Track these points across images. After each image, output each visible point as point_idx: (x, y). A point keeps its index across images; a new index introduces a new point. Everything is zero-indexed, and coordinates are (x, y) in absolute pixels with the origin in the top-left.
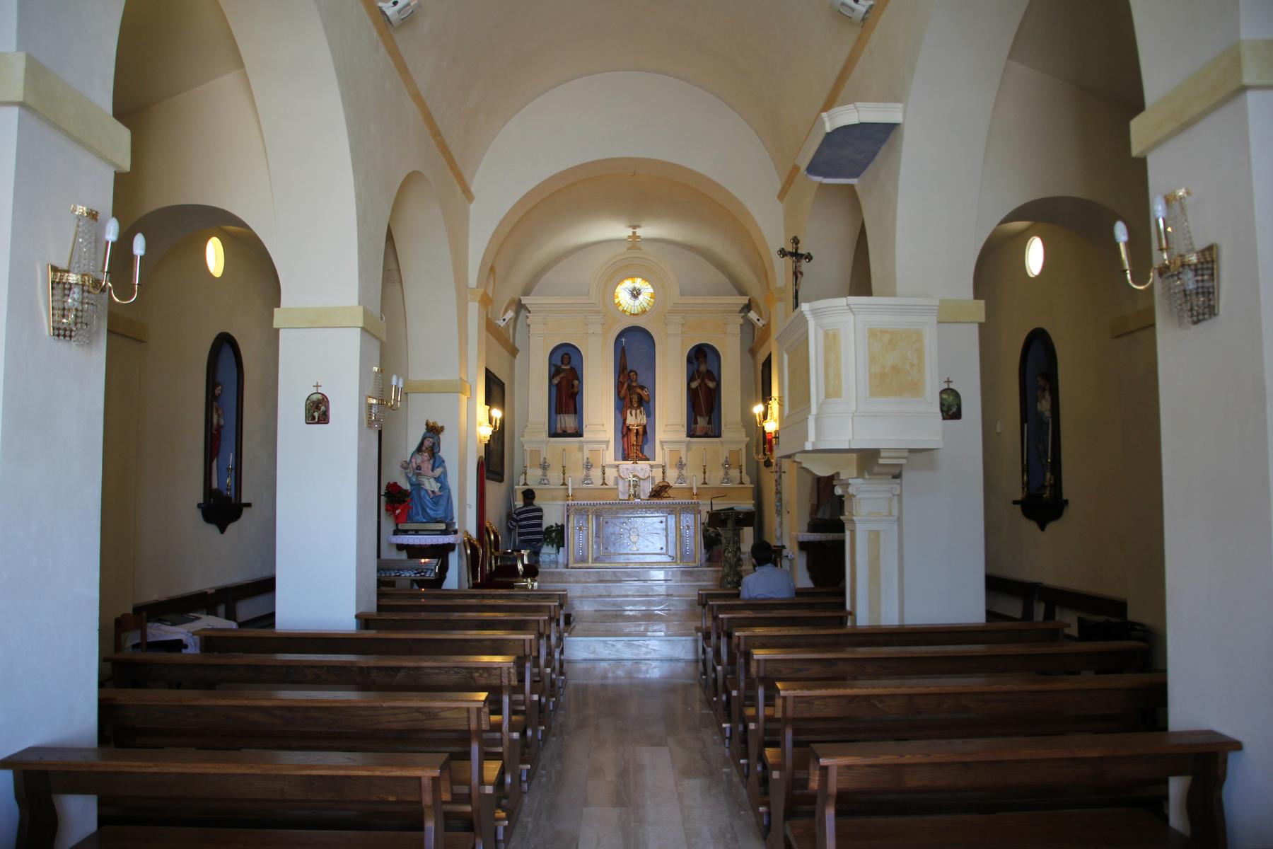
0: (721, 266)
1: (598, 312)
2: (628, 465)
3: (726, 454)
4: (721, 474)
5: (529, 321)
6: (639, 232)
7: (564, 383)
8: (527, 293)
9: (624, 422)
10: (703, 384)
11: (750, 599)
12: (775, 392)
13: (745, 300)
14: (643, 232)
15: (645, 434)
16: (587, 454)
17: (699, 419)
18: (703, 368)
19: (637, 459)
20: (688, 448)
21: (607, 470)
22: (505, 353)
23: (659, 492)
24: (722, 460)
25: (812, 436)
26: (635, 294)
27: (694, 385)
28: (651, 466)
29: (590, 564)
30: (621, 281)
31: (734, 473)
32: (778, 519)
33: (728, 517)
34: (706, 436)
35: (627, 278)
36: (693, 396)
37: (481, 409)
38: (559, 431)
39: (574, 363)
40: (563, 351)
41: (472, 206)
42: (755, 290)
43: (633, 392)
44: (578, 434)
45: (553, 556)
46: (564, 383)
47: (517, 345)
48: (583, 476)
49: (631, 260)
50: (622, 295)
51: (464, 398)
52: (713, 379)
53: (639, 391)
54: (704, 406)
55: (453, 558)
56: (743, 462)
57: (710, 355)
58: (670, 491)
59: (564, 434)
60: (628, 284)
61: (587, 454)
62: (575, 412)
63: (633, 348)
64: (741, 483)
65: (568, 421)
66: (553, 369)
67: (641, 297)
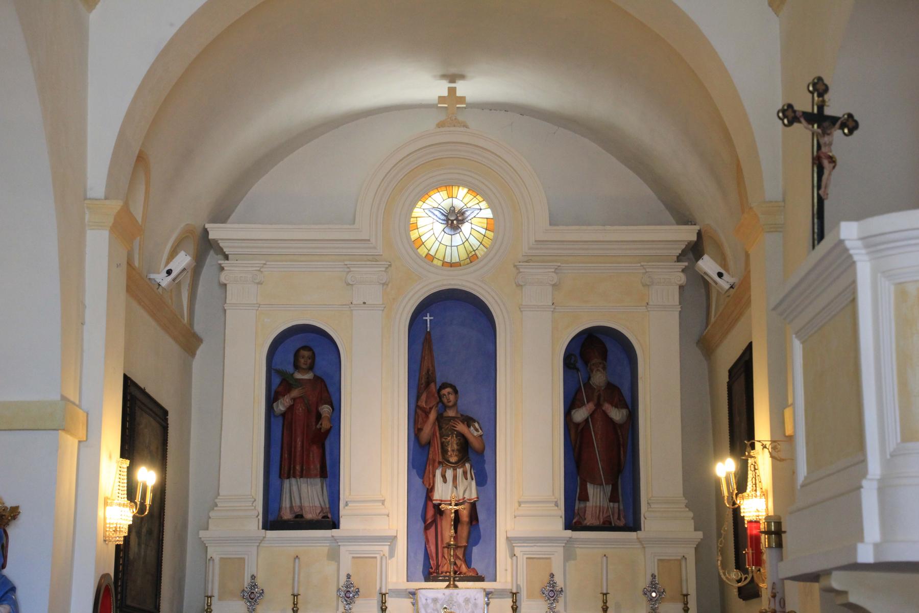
0: (637, 160)
6: (464, 89)
7: (300, 409)
8: (221, 215)
9: (430, 491)
10: (598, 412)
13: (688, 234)
14: (472, 89)
15: (474, 523)
17: (591, 489)
18: (599, 379)
20: (569, 556)
21: (391, 602)
22: (170, 346)
24: (643, 582)
25: (872, 530)
26: (454, 220)
27: (580, 415)
28: (488, 594)
30: (424, 194)
34: (607, 526)
35: (437, 186)
37: (111, 468)
38: (287, 515)
39: (322, 364)
44: (330, 521)
46: (300, 409)
47: (198, 328)
49: (445, 149)
50: (427, 224)
52: (620, 403)
53: (461, 427)
54: (601, 467)
56: (691, 587)
59: (299, 523)
60: (439, 199)
62: (323, 474)
63: (450, 334)
65: (307, 494)
66: (277, 381)
67: (466, 228)
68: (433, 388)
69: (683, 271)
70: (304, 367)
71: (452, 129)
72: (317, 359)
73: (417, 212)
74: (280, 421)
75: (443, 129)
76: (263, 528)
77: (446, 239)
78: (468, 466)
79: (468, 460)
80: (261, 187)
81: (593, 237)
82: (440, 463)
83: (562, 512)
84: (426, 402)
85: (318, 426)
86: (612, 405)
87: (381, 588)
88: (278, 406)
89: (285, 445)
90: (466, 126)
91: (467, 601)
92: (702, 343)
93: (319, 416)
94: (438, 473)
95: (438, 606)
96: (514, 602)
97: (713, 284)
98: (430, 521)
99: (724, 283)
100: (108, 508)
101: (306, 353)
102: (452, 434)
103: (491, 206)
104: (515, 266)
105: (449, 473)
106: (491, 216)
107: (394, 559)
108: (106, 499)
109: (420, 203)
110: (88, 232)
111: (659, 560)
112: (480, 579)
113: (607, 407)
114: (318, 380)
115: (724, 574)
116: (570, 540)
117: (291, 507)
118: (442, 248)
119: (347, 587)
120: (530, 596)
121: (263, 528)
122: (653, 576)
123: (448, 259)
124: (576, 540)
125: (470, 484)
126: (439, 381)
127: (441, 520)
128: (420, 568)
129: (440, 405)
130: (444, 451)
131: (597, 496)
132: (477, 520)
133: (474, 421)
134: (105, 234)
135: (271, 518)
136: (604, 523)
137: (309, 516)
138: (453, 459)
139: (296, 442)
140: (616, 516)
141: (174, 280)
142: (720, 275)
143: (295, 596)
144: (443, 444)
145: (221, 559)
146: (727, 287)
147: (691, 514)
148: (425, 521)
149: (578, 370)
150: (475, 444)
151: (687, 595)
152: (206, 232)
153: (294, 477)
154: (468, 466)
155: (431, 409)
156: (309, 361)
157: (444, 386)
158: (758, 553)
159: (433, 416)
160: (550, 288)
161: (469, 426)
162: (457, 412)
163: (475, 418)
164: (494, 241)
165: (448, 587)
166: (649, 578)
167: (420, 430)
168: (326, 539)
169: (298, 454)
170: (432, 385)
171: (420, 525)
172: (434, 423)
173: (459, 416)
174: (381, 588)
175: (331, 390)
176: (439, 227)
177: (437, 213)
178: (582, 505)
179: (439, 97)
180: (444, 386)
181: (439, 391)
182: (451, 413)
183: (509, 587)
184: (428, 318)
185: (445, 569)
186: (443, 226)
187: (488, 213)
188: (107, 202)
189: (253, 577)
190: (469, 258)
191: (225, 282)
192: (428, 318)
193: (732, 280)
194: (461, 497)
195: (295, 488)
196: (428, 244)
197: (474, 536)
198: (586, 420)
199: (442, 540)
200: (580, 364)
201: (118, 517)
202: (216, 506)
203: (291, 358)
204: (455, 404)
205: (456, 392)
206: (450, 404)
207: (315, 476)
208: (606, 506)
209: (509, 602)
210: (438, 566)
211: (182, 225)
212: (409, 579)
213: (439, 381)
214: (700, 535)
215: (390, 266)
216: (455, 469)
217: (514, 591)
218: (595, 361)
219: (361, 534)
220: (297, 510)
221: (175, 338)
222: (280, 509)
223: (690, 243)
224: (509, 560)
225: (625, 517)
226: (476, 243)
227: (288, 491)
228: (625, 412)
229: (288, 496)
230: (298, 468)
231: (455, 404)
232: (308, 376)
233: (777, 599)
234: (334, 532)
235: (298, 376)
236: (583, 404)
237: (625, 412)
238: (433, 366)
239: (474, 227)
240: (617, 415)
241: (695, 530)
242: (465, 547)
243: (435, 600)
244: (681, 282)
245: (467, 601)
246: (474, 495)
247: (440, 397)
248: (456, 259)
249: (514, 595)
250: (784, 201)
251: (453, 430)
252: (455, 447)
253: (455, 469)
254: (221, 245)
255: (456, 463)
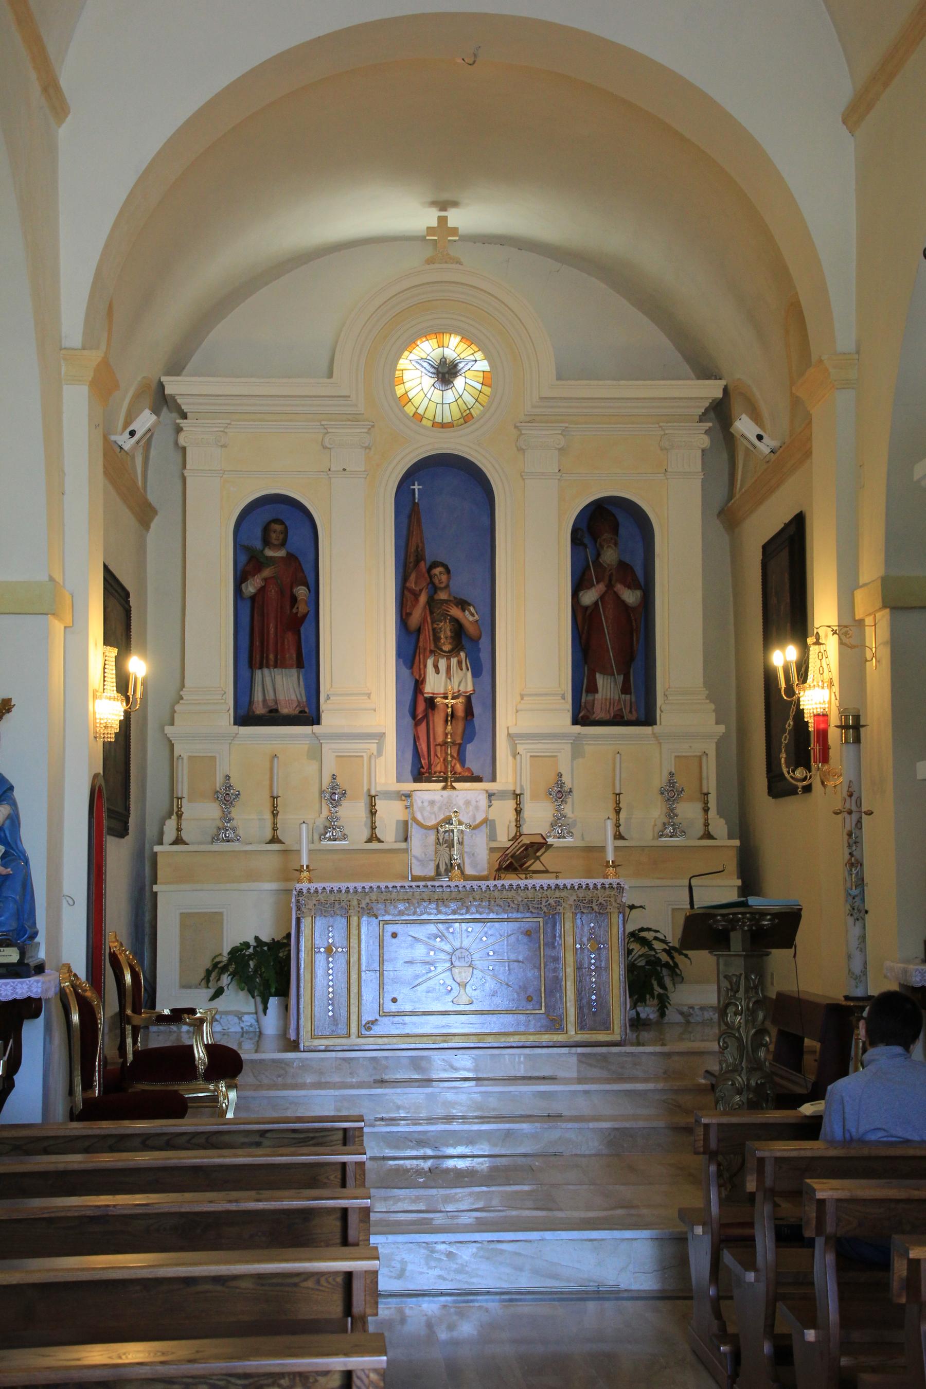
0: (654, 305)
1: (355, 418)
2: (429, 794)
3: (669, 765)
4: (657, 813)
5: (182, 440)
6: (457, 218)
7: (272, 592)
8: (176, 368)
9: (419, 685)
11: (849, 1141)
12: (824, 612)
13: (712, 390)
15: (474, 717)
16: (330, 766)
17: (600, 680)
18: (610, 556)
19: (448, 779)
20: (577, 753)
21: (380, 805)
22: (128, 519)
23: (519, 858)
24: (659, 780)
26: (446, 373)
27: (589, 597)
28: (490, 796)
29: (354, 1040)
30: (410, 343)
31: (689, 811)
32: (856, 931)
33: (733, 923)
34: (618, 720)
35: (425, 334)
36: (585, 625)
37: (98, 656)
38: (260, 710)
39: (297, 539)
40: (265, 515)
41: (63, 131)
42: (749, 360)
43: (441, 613)
44: (309, 715)
45: (249, 1020)
46: (272, 592)
47: (152, 497)
48: (321, 821)
51: (58, 627)
52: (633, 584)
53: (455, 612)
54: (612, 652)
55: (33, 1035)
56: (711, 785)
57: (627, 527)
58: (547, 859)
59: (273, 718)
60: (427, 348)
61: (330, 766)
62: (300, 664)
63: (443, 504)
64: (708, 836)
65: (283, 686)
66: (243, 559)
67: (459, 382)
68: (423, 566)
69: (706, 432)
70: (276, 542)
71: (444, 266)
72: (290, 533)
73: (403, 363)
74: (248, 604)
75: (432, 266)
76: (235, 724)
77: (437, 395)
78: (462, 654)
79: (462, 649)
80: (219, 333)
81: (676, 394)
82: (432, 652)
83: (569, 706)
84: (416, 583)
85: (294, 611)
86: (625, 586)
87: (369, 790)
88: (247, 587)
89: (256, 629)
90: (459, 262)
91: (468, 803)
92: (727, 515)
93: (294, 600)
94: (430, 662)
95: (436, 809)
96: (518, 804)
97: (752, 449)
98: (420, 716)
99: (763, 448)
100: (97, 701)
101: (278, 527)
102: (445, 619)
103: (488, 357)
104: (516, 427)
105: (442, 663)
106: (487, 368)
107: (382, 758)
108: (95, 691)
109: (406, 353)
110: (65, 387)
111: (676, 757)
112: (478, 779)
113: (619, 587)
114: (291, 558)
115: (789, 773)
116: (579, 736)
117: (265, 700)
118: (432, 405)
119: (332, 788)
120: (534, 797)
121: (235, 724)
122: (671, 774)
123: (438, 419)
124: (586, 736)
125: (466, 675)
126: (429, 559)
127: (433, 715)
128: (408, 767)
129: (430, 586)
130: (437, 639)
131: (607, 687)
132: (472, 715)
133: (469, 604)
134: (85, 389)
135: (241, 712)
136: (615, 716)
137: (284, 711)
138: (447, 648)
139: (268, 628)
140: (628, 709)
141: (138, 442)
142: (760, 438)
143: (274, 798)
144: (434, 630)
145: (190, 758)
146: (767, 451)
147: (713, 706)
148: (414, 715)
149: (586, 547)
150: (471, 629)
151: (707, 794)
152: (161, 386)
153: (268, 667)
154: (462, 654)
155: (421, 590)
156: (281, 537)
157: (435, 565)
158: (825, 749)
159: (423, 599)
160: (557, 452)
161: (464, 611)
162: (450, 595)
163: (469, 601)
164: (492, 398)
165: (444, 788)
166: (665, 776)
167: (409, 615)
168: (305, 736)
169: (271, 641)
170: (422, 563)
171: (408, 720)
172: (425, 607)
173: (452, 599)
174: (369, 790)
175: (308, 568)
176: (428, 381)
177: (425, 365)
178: (590, 697)
179: (428, 228)
180: (435, 565)
181: (429, 570)
182: (443, 596)
183: (511, 787)
184: (416, 487)
185: (438, 768)
186: (433, 381)
187: (484, 365)
188: (86, 352)
189: (228, 777)
190: (463, 417)
191: (185, 444)
192: (416, 487)
193: (774, 444)
194: (456, 690)
195: (268, 680)
196: (416, 402)
197: (469, 734)
198: (596, 603)
199: (434, 738)
200: (587, 540)
201: (108, 711)
202: (182, 698)
203: (259, 532)
204: (447, 586)
205: (448, 571)
206: (442, 586)
207: (291, 667)
208: (617, 698)
209: (511, 804)
210: (430, 765)
211: (139, 379)
212: (398, 781)
213: (429, 559)
214: (722, 729)
215: (373, 426)
216: (448, 659)
217: (518, 792)
218: (606, 536)
219: (346, 730)
220: (271, 704)
221: (131, 508)
222: (251, 702)
223: (714, 400)
224: (510, 758)
225: (641, 711)
226: (470, 400)
227: (260, 683)
228: (638, 593)
229: (260, 689)
230: (271, 657)
231: (447, 586)
232: (281, 553)
233: (854, 798)
234: (316, 728)
235: (269, 553)
236: (592, 585)
237: (638, 593)
238: (423, 543)
239: (468, 381)
240: (630, 597)
241: (717, 723)
242: (460, 745)
243: (432, 803)
244: (703, 446)
245: (468, 803)
246: (470, 688)
247: (431, 577)
248: (447, 419)
249: (517, 796)
250: (858, 352)
251: (445, 615)
252: (449, 633)
253: (448, 659)
254: (179, 401)
255: (449, 652)
